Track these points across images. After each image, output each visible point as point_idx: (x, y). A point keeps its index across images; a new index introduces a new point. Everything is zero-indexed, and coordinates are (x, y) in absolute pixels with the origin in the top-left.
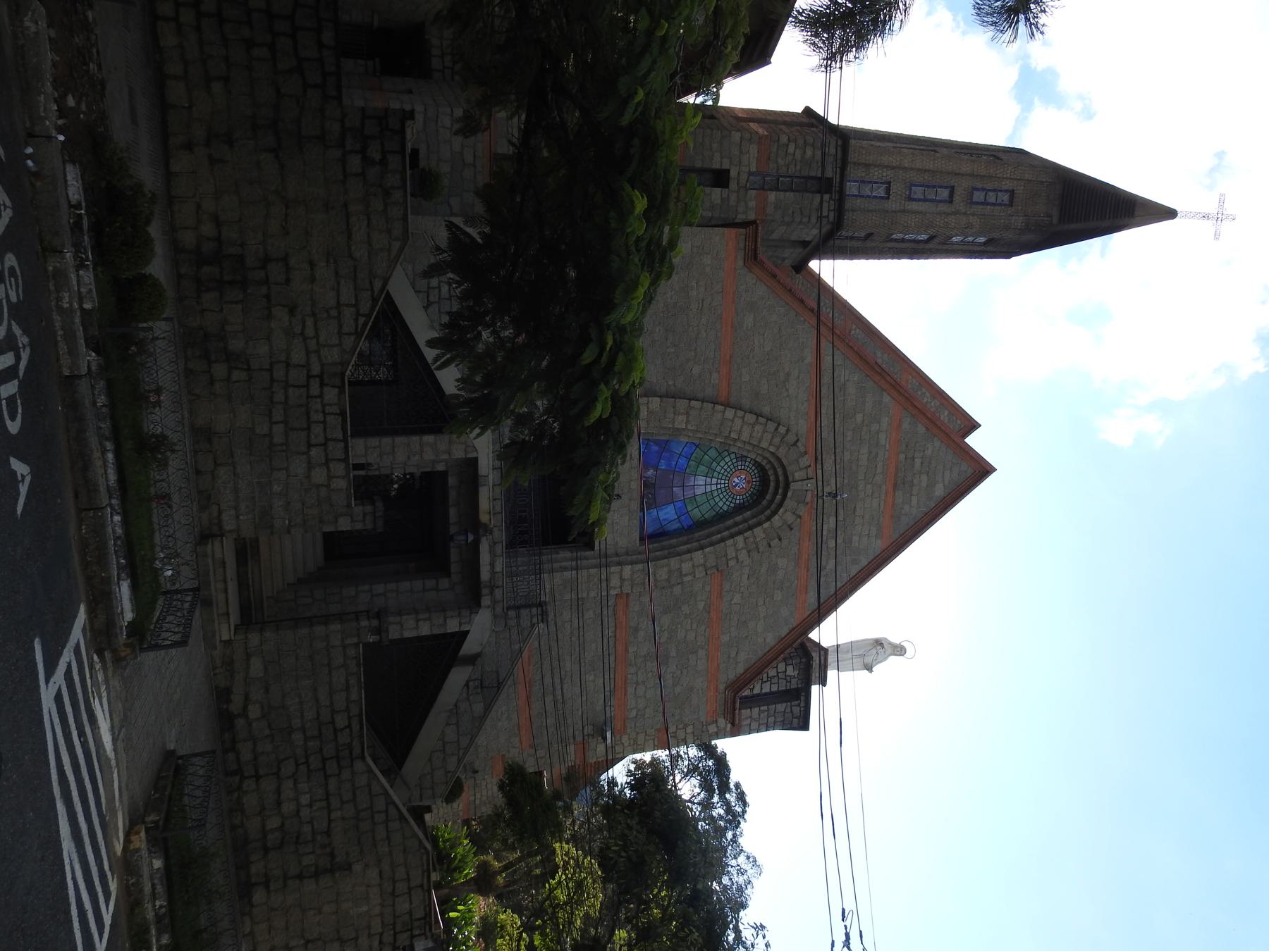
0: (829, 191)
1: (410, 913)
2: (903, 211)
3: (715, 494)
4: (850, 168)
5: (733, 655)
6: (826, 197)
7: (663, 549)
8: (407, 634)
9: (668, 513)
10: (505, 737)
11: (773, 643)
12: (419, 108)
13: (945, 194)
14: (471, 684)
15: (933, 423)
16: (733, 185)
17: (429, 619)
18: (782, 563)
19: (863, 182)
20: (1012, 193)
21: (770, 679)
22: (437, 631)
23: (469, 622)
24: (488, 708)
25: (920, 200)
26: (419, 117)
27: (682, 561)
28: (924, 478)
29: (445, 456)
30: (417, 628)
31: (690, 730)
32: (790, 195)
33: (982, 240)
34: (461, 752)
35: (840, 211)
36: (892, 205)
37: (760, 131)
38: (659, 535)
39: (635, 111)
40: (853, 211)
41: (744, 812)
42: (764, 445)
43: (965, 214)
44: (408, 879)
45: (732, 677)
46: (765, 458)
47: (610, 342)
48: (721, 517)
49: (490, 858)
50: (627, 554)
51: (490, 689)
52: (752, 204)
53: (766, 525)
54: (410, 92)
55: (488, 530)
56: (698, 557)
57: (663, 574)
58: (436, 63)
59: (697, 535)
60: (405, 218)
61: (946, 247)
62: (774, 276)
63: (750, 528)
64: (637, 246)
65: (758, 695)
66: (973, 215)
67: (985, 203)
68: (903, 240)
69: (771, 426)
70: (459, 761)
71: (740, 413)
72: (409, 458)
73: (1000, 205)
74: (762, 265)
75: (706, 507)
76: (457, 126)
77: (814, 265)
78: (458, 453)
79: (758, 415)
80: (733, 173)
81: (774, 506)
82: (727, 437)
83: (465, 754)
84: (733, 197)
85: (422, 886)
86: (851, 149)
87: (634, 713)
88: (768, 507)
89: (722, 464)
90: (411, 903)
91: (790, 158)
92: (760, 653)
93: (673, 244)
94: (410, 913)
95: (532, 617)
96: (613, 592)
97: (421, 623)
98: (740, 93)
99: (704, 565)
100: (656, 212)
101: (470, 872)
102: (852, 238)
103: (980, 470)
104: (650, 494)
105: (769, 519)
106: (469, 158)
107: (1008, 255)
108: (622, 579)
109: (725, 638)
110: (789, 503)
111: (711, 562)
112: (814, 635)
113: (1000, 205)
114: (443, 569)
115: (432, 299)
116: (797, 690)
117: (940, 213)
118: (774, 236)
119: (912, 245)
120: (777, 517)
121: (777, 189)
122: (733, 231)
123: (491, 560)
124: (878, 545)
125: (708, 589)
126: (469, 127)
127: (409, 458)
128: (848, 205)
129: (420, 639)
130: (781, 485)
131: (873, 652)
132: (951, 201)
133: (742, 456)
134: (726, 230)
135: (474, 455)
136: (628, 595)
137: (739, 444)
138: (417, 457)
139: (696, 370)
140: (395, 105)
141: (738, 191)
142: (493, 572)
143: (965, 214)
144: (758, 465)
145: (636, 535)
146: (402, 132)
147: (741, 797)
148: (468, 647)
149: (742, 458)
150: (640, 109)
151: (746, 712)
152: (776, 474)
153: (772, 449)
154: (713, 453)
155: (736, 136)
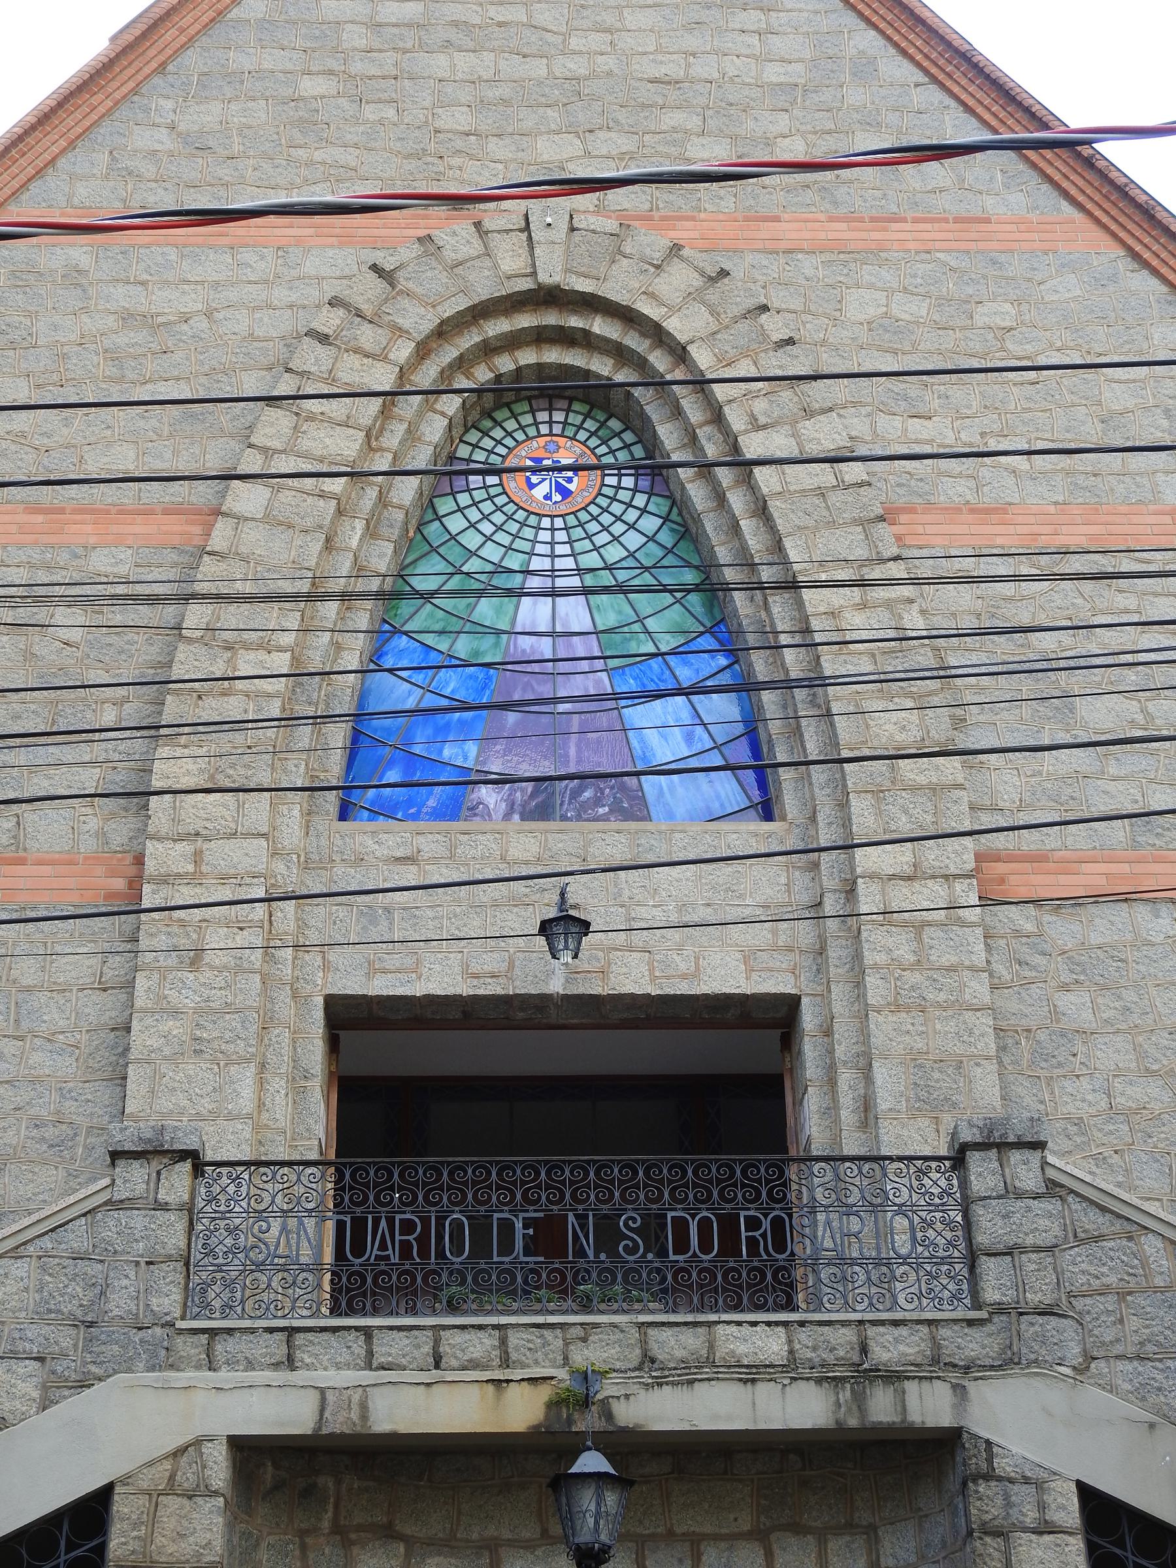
55: (580, 1395)
81: (634, 341)
89: (472, 540)
95: (1011, 1192)
98: (613, 1472)
110: (618, 287)
120: (673, 325)
130: (551, 318)
135: (218, 1468)
142: (790, 1370)
152: (512, 342)
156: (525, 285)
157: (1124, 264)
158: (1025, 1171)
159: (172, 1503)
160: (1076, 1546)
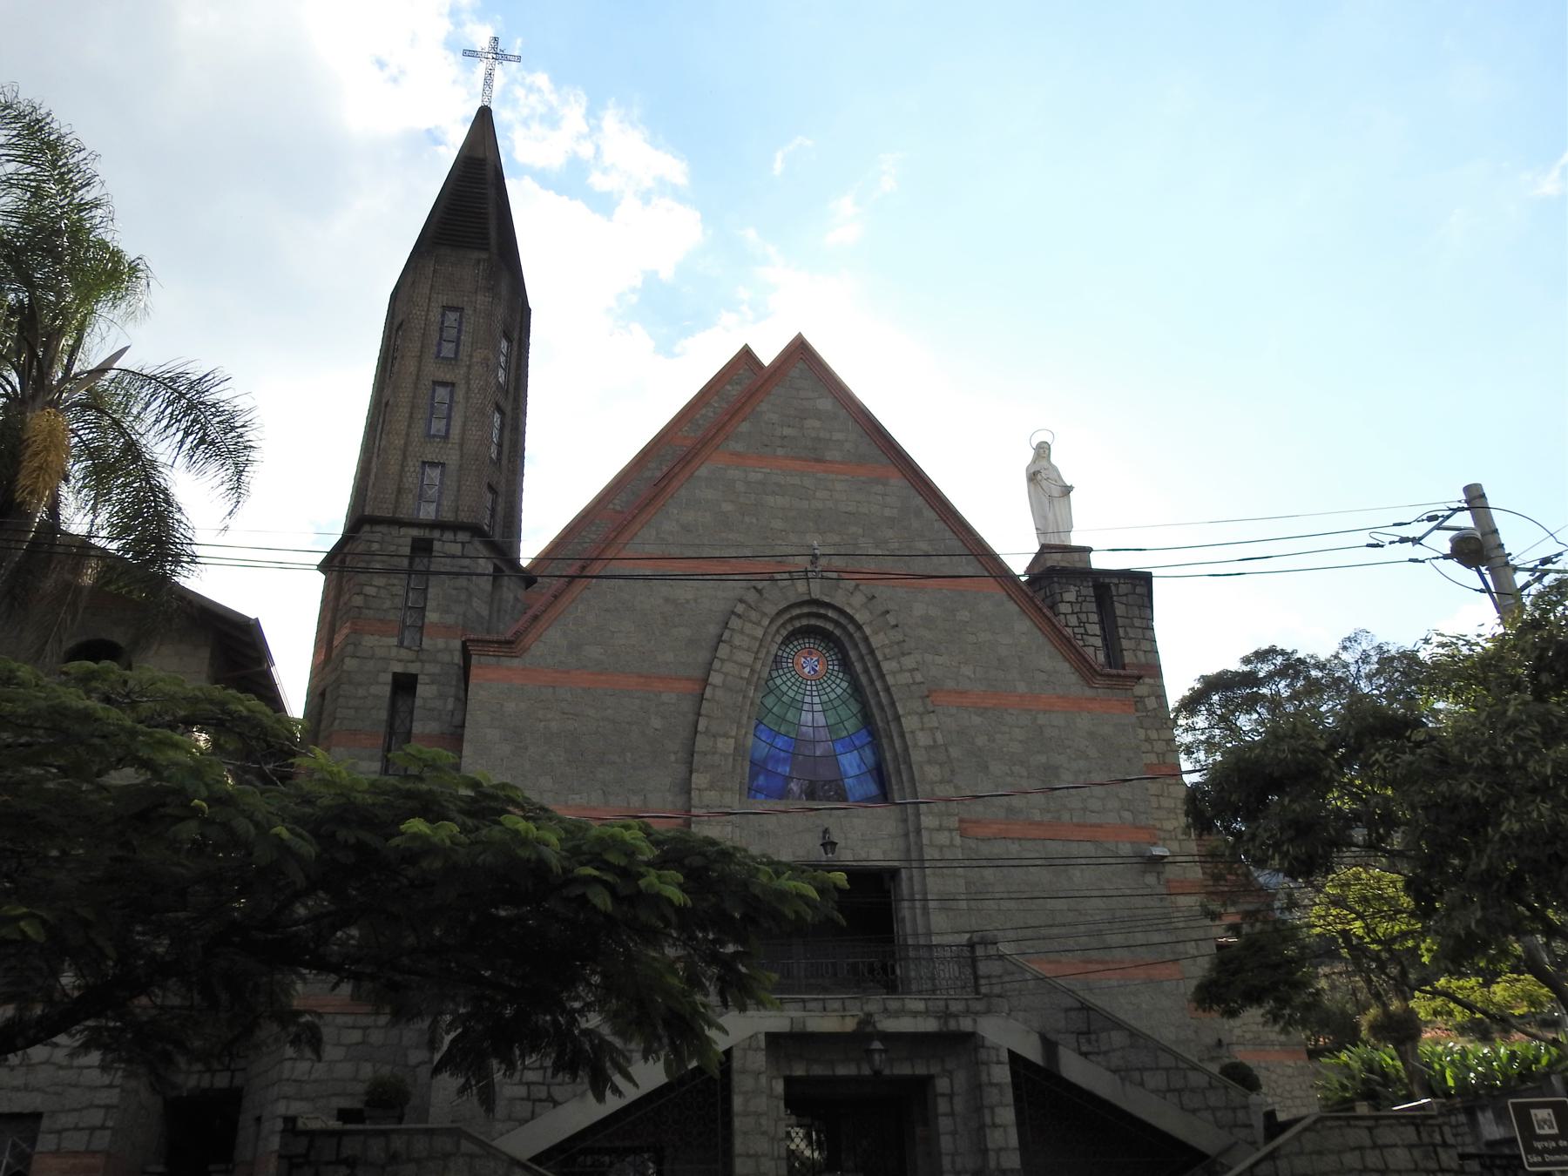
0: (430, 542)
1: (1410, 1147)
2: (461, 445)
3: (825, 698)
4: (403, 514)
5: (1044, 677)
6: (437, 545)
7: (899, 772)
8: (1014, 1141)
9: (851, 763)
10: (1158, 1001)
11: (1028, 623)
12: (282, 1108)
13: (442, 393)
14: (1084, 1049)
15: (736, 411)
16: (413, 668)
17: (992, 1109)
18: (919, 609)
19: (420, 497)
20: (447, 308)
21: (1081, 624)
22: (1009, 1097)
23: (997, 1049)
24: (1118, 1025)
25: (448, 425)
26: (296, 1108)
27: (916, 745)
28: (810, 423)
29: (763, 1080)
30: (1005, 1127)
31: (1153, 735)
32: (432, 592)
33: (504, 345)
34: (1182, 1065)
35: (456, 527)
36: (452, 459)
37: (345, 631)
38: (879, 774)
39: (300, 836)
40: (457, 509)
41: (1283, 653)
42: (759, 633)
43: (469, 367)
44: (1361, 1148)
45: (1074, 678)
46: (778, 631)
47: (589, 871)
48: (856, 689)
49: (1364, 1021)
50: (905, 821)
51: (1090, 1022)
52: (441, 643)
53: (868, 631)
54: (259, 1119)
55: (867, 1020)
56: (909, 723)
57: (933, 772)
58: (221, 1081)
59: (880, 724)
60: (430, 1132)
61: (511, 389)
62: (536, 618)
63: (872, 652)
64: (470, 832)
65: (1104, 639)
66: (471, 356)
67: (458, 342)
68: (500, 445)
69: (735, 623)
70: (1194, 1068)
71: (717, 664)
72: (764, 1133)
73: (460, 323)
74: (518, 635)
75: (843, 711)
76: (308, 1053)
77: (524, 563)
78: (759, 1060)
79: (720, 640)
80: (399, 668)
81: (843, 620)
82: (749, 682)
83: (1185, 1060)
84: (431, 668)
85: (1370, 1129)
86: (377, 513)
87: (1127, 815)
88: (844, 628)
89: (784, 688)
90: (1395, 1146)
91: (383, 593)
92: (1041, 639)
93: (475, 785)
94: (1410, 1147)
95: (989, 957)
96: (958, 840)
97: (998, 1121)
99: (921, 715)
100: (430, 809)
101: (1387, 1056)
102: (493, 510)
103: (799, 351)
104: (824, 789)
105: (859, 627)
106: (356, 1036)
107: (526, 312)
108: (940, 829)
109: (1022, 687)
111: (917, 705)
112: (1019, 564)
113: (460, 323)
114: (923, 1084)
115: (544, 1095)
116: (1095, 587)
117: (467, 399)
118: (485, 613)
119: (507, 433)
120: (857, 617)
121: (423, 609)
122: (473, 671)
123: (908, 1017)
124: (897, 482)
125: (953, 711)
126: (311, 1039)
127: (764, 1133)
128: (448, 516)
129: (1020, 1124)
130: (814, 610)
131: (1046, 485)
132: (451, 385)
133: (775, 661)
134: (472, 681)
135: (762, 1038)
136: (961, 821)
137: (758, 666)
138: (764, 1121)
139: (656, 723)
140: (275, 1143)
141: (422, 662)
142: (927, 1013)
143: (469, 367)
144: (787, 641)
145: (881, 810)
146: (312, 1134)
147: (1262, 656)
148: (1032, 1052)
149: (777, 661)
150: (299, 830)
151: (1128, 657)
152: (799, 617)
153: (766, 622)
154: (769, 702)
155: (350, 664)
156: (806, 598)
157: (1005, 598)
158: (992, 951)
159: (750, 1053)
160: (1007, 1067)
